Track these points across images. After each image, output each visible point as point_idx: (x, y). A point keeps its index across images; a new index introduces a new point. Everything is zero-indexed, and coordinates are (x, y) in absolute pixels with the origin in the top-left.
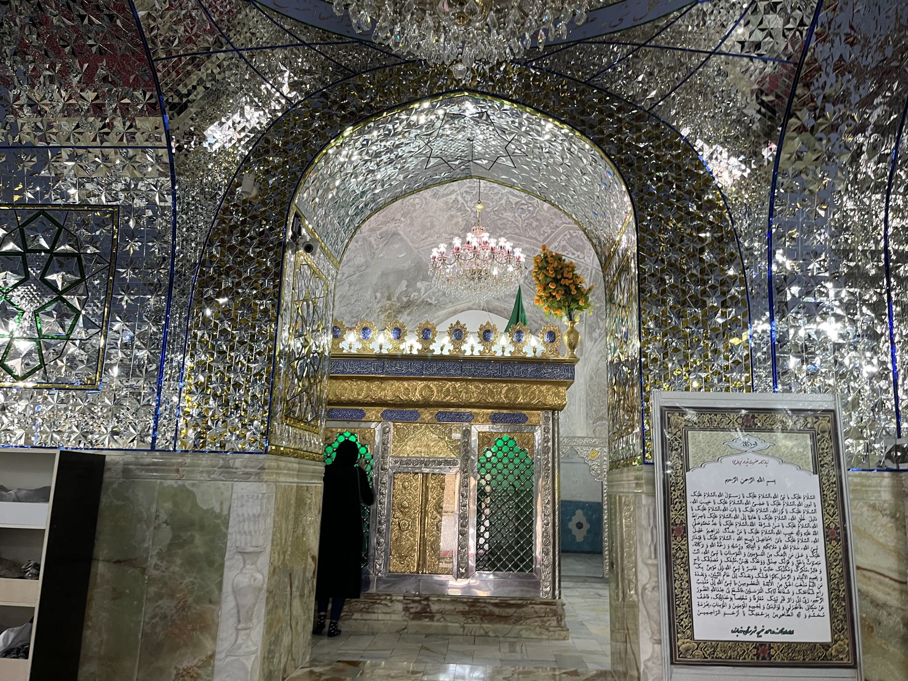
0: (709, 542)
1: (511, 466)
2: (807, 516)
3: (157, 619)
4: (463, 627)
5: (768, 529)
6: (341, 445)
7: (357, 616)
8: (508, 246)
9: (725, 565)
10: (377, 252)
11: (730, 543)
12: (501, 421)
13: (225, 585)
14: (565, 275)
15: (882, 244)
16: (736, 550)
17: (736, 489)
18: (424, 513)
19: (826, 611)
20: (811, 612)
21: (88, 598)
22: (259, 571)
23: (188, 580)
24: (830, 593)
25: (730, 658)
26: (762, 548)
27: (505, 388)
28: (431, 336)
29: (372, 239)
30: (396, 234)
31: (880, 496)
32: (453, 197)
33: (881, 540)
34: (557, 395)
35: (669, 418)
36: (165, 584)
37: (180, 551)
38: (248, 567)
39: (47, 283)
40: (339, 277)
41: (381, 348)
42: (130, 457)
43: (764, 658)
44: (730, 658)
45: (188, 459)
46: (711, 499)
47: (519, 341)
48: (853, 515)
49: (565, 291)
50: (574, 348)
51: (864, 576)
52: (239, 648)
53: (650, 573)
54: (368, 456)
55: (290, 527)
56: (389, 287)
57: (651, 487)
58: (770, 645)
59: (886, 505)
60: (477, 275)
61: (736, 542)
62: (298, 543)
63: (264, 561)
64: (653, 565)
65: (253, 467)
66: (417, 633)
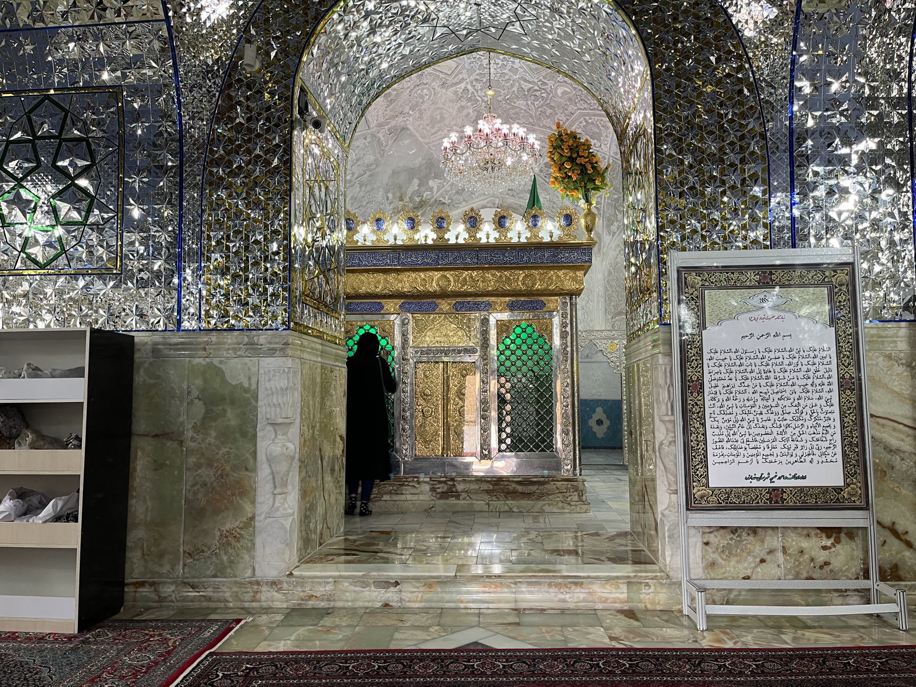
2: (822, 368)
3: (198, 486)
4: (488, 504)
5: (783, 381)
6: (362, 337)
7: (386, 497)
8: (521, 132)
10: (387, 149)
11: (746, 396)
13: (259, 454)
14: (580, 154)
16: (751, 403)
17: (750, 345)
18: (446, 400)
19: (839, 456)
21: (131, 470)
23: (224, 450)
24: (843, 440)
25: (744, 503)
26: (776, 400)
27: (521, 274)
28: (445, 225)
29: (380, 135)
30: (404, 129)
31: (896, 347)
33: (896, 389)
34: (574, 279)
35: (686, 278)
36: (203, 454)
37: (214, 424)
38: (279, 437)
40: (348, 178)
41: (395, 239)
43: (777, 502)
44: (744, 503)
47: (535, 225)
48: (868, 365)
49: (582, 170)
50: (591, 231)
51: (878, 423)
52: (277, 510)
53: (667, 430)
54: (389, 348)
55: (317, 404)
56: (400, 187)
57: (667, 347)
58: (782, 490)
59: (902, 355)
60: (491, 165)
61: (751, 395)
62: (326, 429)
63: (294, 431)
64: (670, 421)
65: (277, 343)
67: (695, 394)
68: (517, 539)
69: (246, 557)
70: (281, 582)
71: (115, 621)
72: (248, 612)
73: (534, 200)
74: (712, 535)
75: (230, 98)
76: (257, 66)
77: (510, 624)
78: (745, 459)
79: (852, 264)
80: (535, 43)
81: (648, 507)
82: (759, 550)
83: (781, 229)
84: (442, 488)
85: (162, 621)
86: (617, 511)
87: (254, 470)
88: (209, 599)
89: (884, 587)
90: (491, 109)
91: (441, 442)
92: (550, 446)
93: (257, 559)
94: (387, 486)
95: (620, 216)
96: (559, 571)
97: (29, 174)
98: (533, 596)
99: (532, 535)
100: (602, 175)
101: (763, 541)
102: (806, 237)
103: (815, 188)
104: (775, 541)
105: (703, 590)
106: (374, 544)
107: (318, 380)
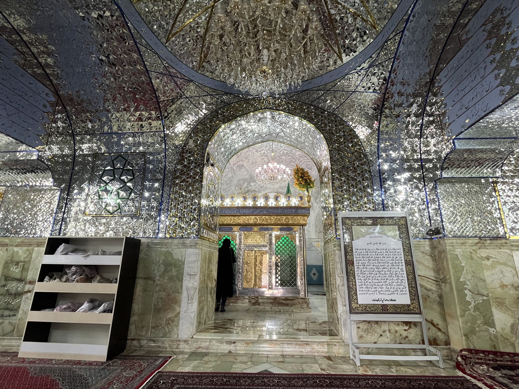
0: (362, 267)
1: (287, 247)
2: (398, 256)
7: (231, 304)
9: (368, 275)
11: (370, 267)
12: (283, 230)
17: (371, 247)
18: (256, 265)
20: (402, 293)
27: (284, 218)
29: (234, 168)
32: (263, 151)
34: (304, 220)
42: (149, 240)
45: (170, 241)
46: (362, 251)
58: (387, 305)
63: (197, 278)
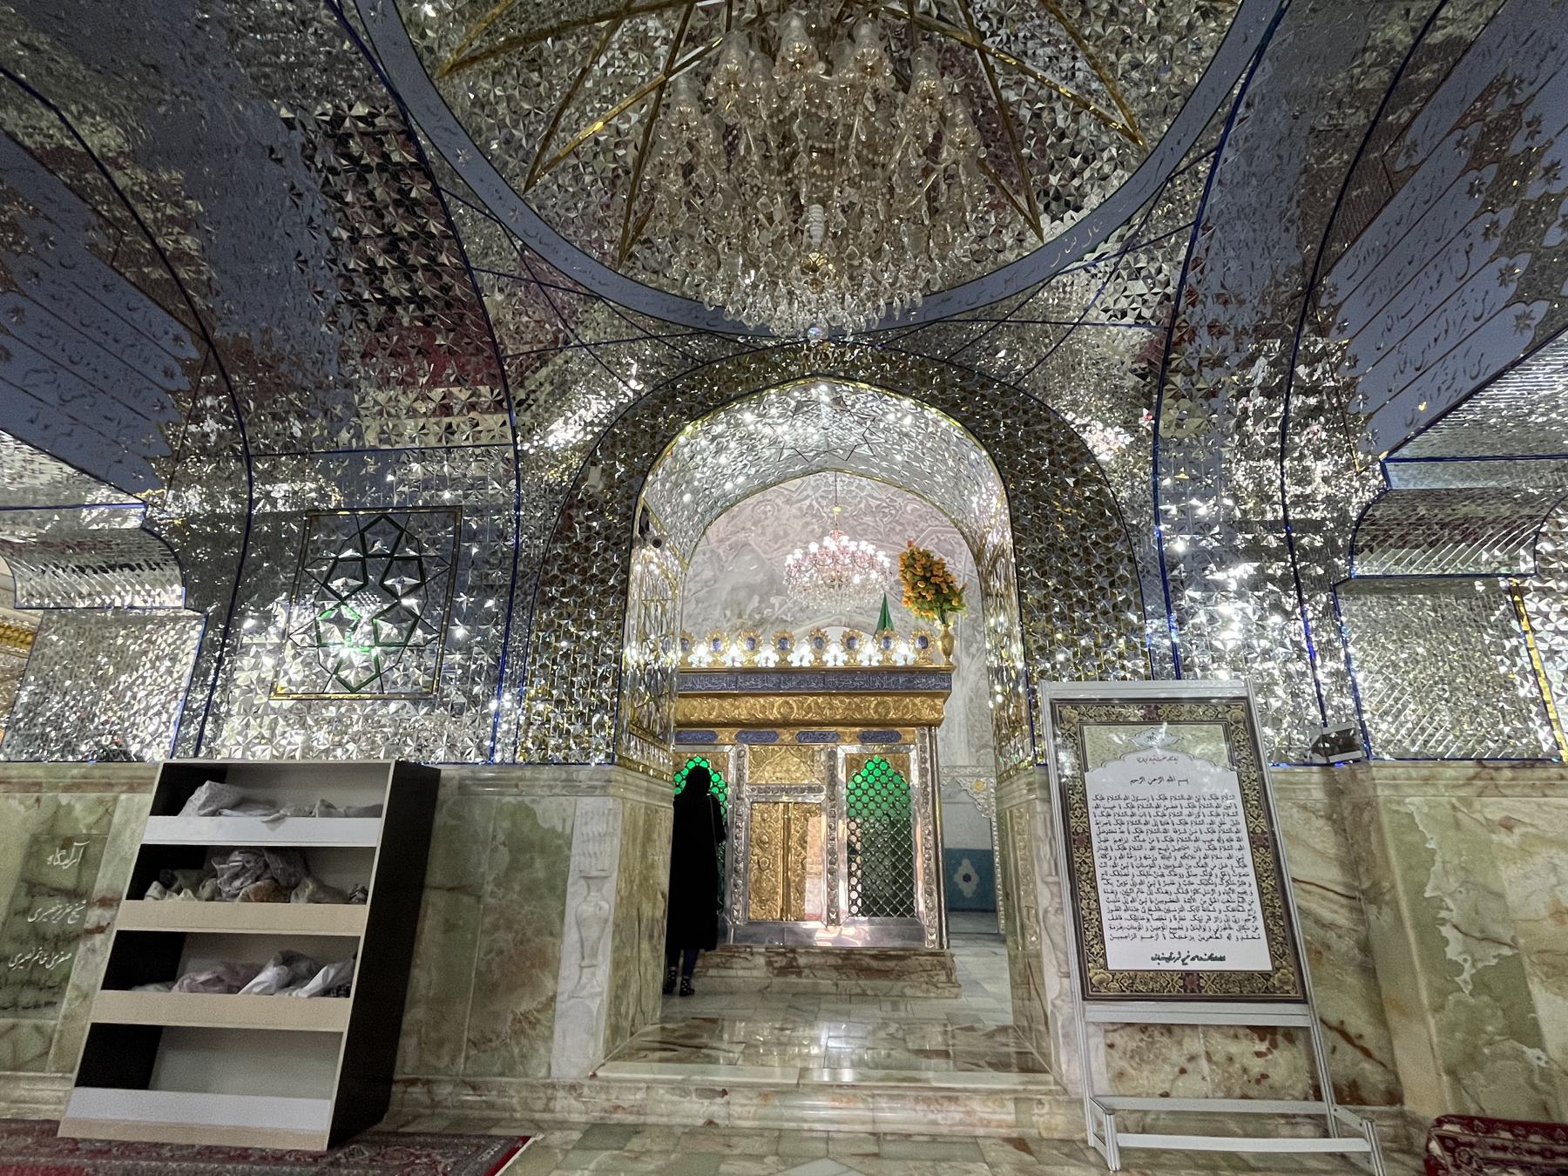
7: (712, 972)
9: (1137, 880)
11: (1142, 853)
15: (1281, 514)
16: (1149, 862)
17: (1142, 790)
18: (787, 849)
19: (1262, 932)
22: (603, 898)
27: (873, 701)
29: (720, 551)
30: (746, 544)
32: (807, 502)
33: (1318, 847)
34: (933, 708)
39: (387, 589)
45: (528, 773)
46: (1116, 803)
47: (887, 648)
52: (583, 988)
58: (1197, 975)
60: (838, 583)
61: (1149, 853)
63: (610, 888)
66: (782, 992)
67: (1082, 850)
68: (874, 1032)
69: (542, 1051)
70: (582, 1086)
71: (377, 1133)
72: (539, 1126)
73: (885, 621)
74: (1116, 1035)
75: (570, 517)
76: (601, 487)
77: (867, 1155)
78: (1149, 934)
79: (1246, 698)
80: (884, 464)
81: (1033, 992)
82: (1177, 1056)
83: (1163, 659)
84: (780, 962)
85: (432, 1135)
86: (994, 996)
87: (560, 935)
88: (491, 1106)
89: (1343, 1113)
90: (838, 525)
91: (780, 902)
92: (910, 910)
93: (554, 1052)
94: (714, 957)
95: (979, 637)
96: (927, 1081)
97: (354, 592)
98: (897, 1115)
99: (892, 1028)
100: (959, 595)
101: (1180, 1043)
102: (1189, 668)
103: (1193, 615)
104: (1195, 1045)
105: (1111, 1111)
106: (696, 1036)
107: (641, 823)
